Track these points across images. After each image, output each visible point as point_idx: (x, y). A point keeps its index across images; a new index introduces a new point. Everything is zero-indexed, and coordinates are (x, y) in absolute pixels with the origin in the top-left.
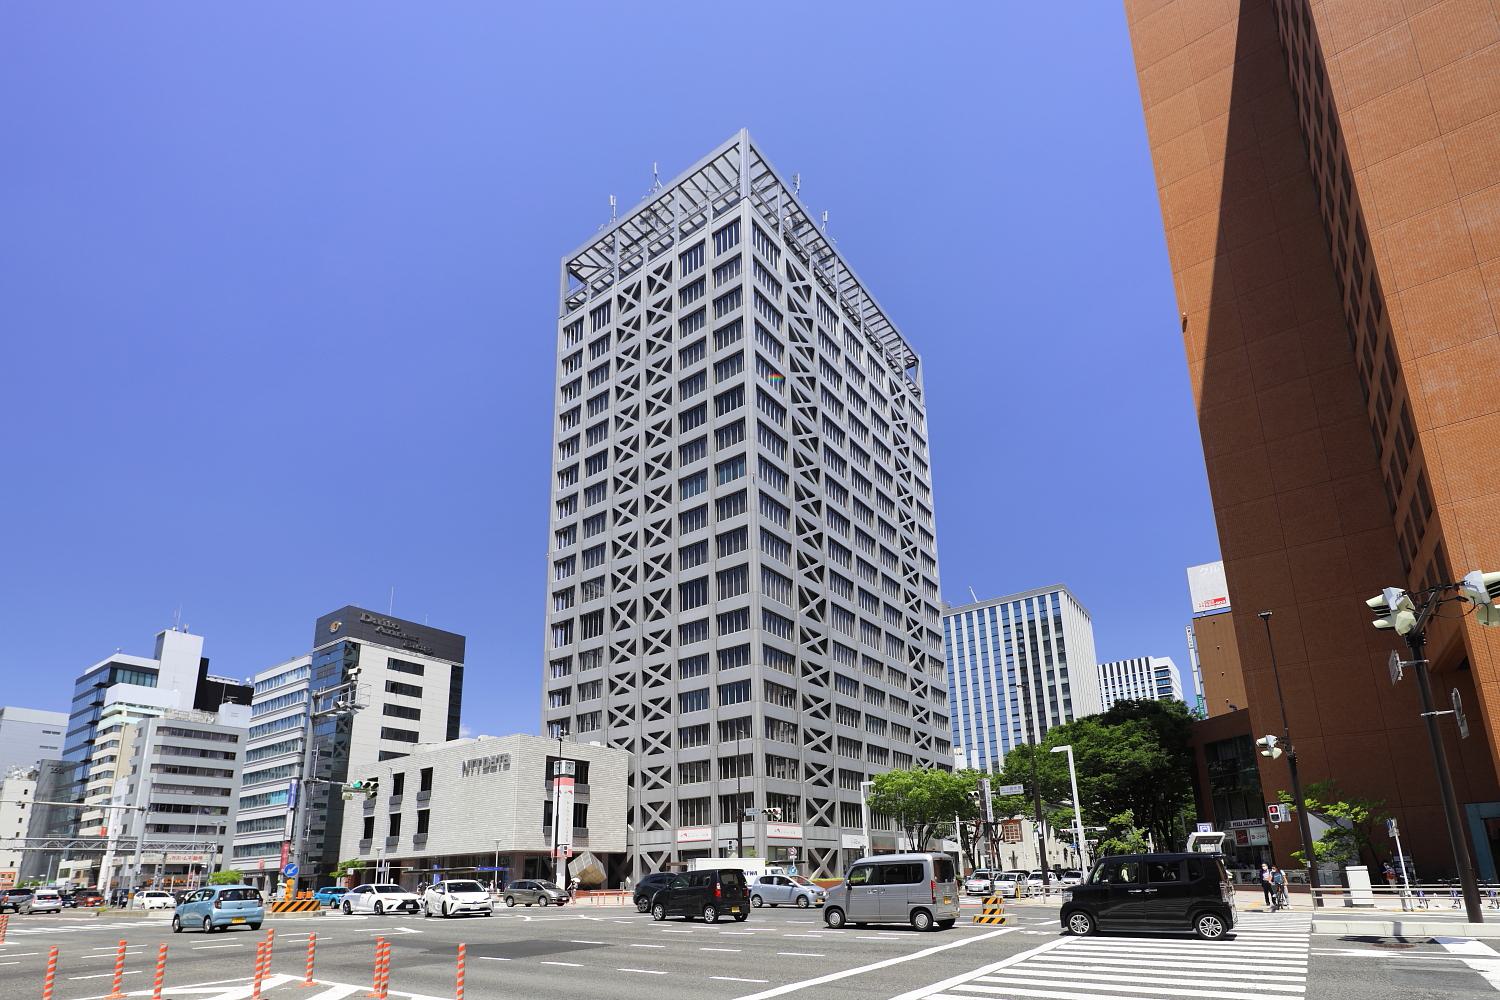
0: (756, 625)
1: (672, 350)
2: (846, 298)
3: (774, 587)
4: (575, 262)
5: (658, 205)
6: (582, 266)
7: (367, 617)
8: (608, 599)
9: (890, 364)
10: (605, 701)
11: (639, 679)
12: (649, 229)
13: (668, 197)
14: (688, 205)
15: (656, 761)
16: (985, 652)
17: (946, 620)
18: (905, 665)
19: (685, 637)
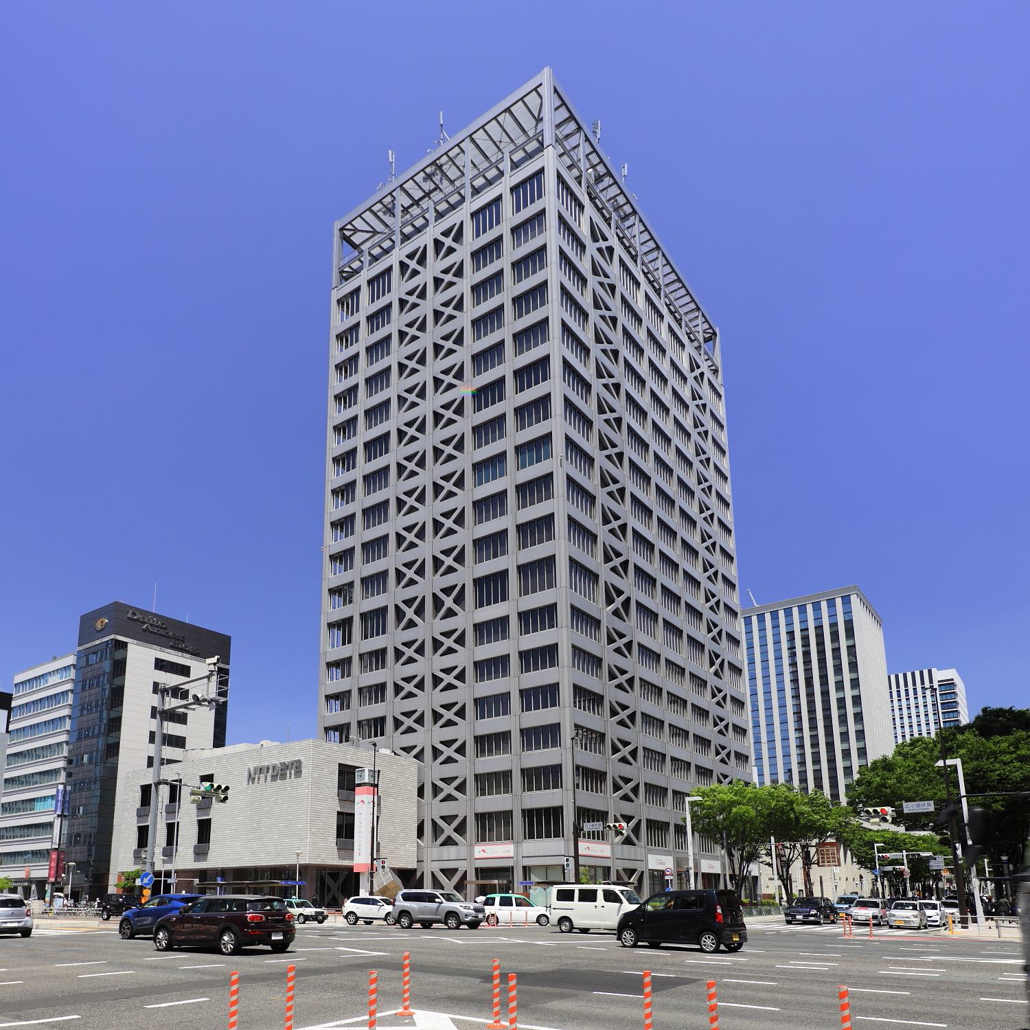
0: (564, 625)
1: (464, 320)
2: (647, 261)
3: (581, 582)
4: (349, 227)
5: (445, 159)
6: (356, 230)
7: (134, 614)
8: (393, 596)
9: (689, 338)
10: (390, 707)
11: (428, 683)
12: (433, 186)
13: (457, 150)
14: (479, 159)
15: (449, 770)
16: (765, 661)
17: (748, 621)
18: (706, 672)
19: (482, 637)
